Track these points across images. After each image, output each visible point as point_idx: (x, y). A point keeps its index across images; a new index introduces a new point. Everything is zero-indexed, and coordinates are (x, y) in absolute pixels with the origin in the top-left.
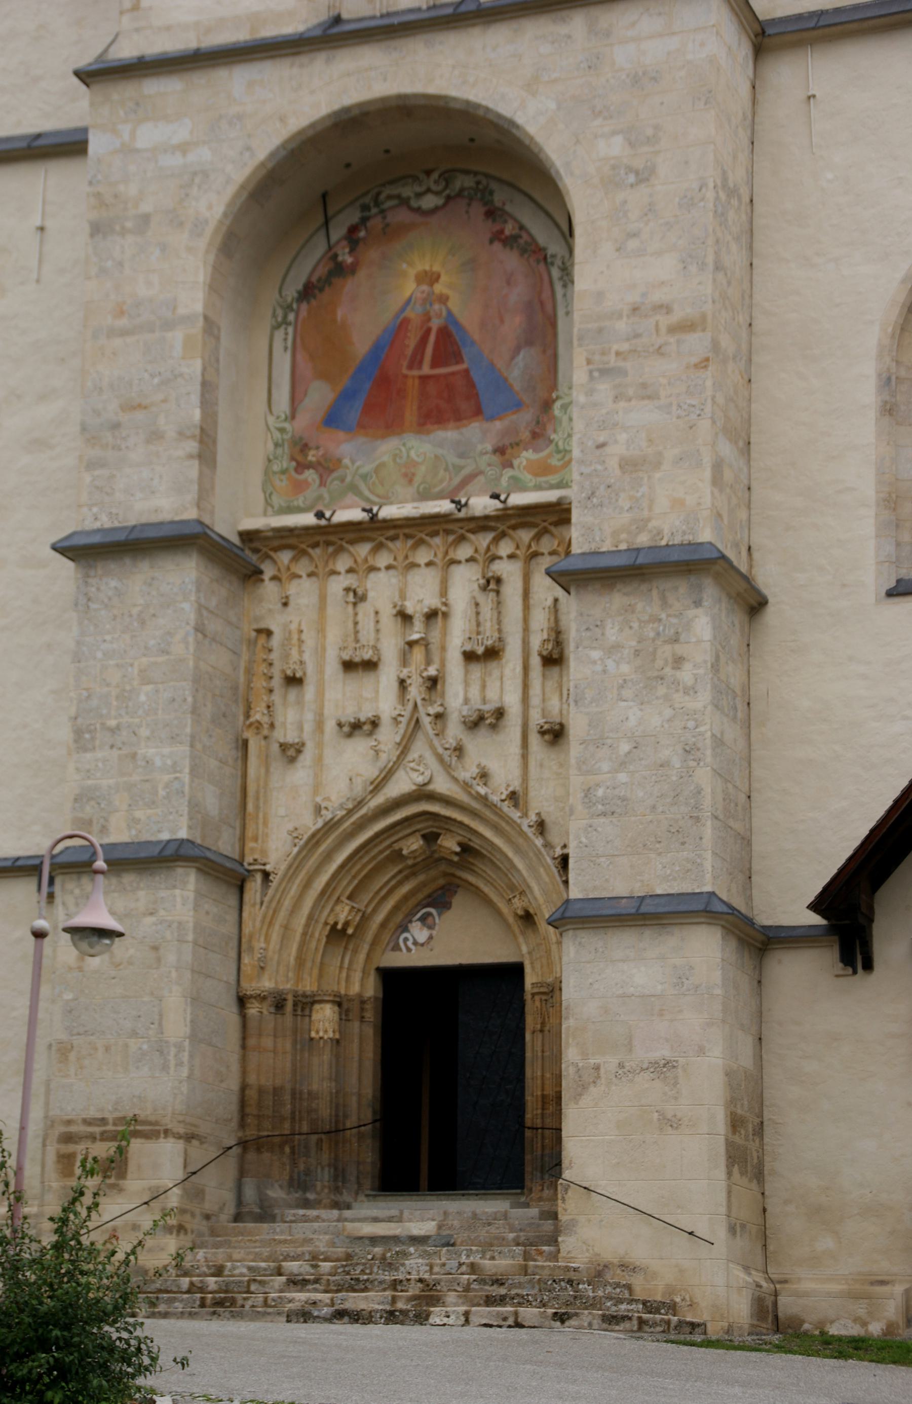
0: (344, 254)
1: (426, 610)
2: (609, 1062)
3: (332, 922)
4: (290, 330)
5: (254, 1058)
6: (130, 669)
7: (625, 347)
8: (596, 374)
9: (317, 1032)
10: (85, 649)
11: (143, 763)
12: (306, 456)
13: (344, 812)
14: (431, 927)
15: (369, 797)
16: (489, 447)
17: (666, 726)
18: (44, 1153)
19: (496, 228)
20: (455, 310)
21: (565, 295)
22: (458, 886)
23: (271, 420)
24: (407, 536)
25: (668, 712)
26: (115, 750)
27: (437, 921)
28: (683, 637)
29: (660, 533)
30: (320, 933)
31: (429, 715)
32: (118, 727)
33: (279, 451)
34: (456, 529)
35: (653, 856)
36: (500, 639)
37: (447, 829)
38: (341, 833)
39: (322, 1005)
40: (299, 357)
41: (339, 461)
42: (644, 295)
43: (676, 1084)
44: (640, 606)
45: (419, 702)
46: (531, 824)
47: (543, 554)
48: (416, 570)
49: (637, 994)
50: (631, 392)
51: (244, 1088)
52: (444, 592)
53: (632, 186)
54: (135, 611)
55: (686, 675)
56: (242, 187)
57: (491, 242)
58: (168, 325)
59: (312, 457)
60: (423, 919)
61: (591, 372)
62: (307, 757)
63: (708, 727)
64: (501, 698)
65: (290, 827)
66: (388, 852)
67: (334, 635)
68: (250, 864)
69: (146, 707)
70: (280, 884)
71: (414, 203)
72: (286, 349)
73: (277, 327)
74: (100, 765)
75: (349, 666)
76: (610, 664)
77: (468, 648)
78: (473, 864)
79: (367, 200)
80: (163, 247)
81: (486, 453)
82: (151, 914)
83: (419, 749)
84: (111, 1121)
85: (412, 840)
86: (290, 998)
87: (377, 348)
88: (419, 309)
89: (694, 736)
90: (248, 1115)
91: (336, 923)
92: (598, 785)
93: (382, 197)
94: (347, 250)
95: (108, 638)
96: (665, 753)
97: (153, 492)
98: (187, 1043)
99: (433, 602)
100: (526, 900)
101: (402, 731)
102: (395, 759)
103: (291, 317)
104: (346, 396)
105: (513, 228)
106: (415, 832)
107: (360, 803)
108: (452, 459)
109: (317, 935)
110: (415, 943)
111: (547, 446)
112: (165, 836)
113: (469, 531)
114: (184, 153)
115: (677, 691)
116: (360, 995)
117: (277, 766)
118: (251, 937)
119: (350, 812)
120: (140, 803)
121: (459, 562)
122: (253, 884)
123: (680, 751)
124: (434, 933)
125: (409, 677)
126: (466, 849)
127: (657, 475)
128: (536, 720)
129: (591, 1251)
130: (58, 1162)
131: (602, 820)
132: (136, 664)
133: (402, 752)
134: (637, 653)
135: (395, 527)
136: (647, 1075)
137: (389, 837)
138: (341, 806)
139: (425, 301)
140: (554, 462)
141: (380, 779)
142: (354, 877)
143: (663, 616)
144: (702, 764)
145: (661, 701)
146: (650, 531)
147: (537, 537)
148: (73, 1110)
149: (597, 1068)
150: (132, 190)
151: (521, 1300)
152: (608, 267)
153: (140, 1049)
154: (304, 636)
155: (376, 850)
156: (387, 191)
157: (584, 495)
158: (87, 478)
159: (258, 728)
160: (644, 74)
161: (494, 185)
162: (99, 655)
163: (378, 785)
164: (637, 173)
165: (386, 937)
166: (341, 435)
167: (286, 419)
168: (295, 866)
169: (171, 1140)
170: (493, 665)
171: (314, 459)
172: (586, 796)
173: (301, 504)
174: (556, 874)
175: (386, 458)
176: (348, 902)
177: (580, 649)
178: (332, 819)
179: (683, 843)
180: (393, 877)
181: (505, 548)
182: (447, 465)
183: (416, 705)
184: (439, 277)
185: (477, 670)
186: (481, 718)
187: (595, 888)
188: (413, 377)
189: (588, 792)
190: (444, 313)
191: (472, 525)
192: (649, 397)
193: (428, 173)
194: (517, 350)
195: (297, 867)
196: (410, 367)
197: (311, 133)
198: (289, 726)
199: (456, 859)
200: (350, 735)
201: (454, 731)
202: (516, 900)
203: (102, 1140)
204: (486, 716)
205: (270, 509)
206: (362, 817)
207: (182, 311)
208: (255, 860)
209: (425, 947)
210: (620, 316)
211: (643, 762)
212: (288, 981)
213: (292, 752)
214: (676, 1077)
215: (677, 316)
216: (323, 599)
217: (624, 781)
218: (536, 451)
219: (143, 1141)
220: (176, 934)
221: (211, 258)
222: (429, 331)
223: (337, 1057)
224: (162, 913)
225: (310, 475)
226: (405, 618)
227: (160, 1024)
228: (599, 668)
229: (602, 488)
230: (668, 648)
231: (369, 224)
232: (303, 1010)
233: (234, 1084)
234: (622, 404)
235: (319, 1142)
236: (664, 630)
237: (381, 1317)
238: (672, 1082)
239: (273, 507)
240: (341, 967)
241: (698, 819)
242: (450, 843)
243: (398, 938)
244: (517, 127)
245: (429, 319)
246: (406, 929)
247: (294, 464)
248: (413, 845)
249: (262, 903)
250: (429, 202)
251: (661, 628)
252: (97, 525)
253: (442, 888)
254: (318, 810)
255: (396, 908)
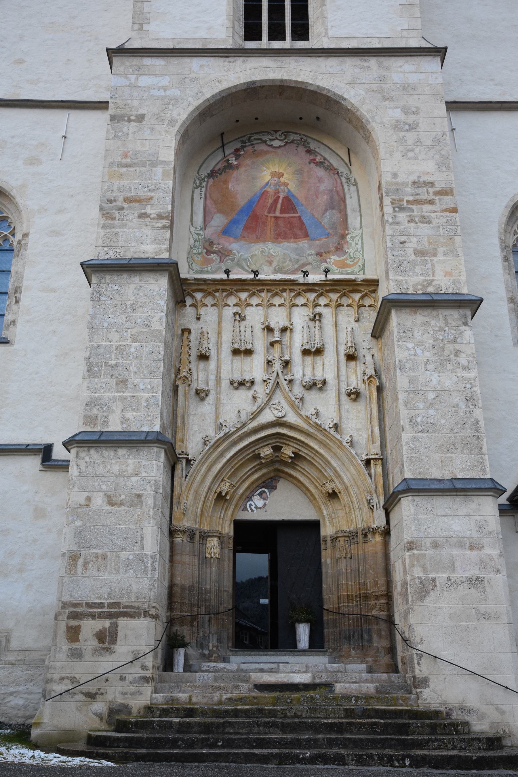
0: (232, 160)
1: (281, 327)
2: (441, 577)
3: (218, 492)
4: (203, 190)
5: (179, 568)
6: (125, 334)
7: (411, 198)
8: (397, 209)
9: (210, 554)
10: (96, 321)
11: (132, 386)
12: (213, 247)
13: (235, 429)
14: (264, 499)
15: (249, 422)
16: (313, 252)
17: (454, 386)
18: (56, 625)
19: (312, 157)
20: (292, 190)
21: (349, 190)
22: (280, 478)
23: (192, 229)
24: (269, 291)
25: (455, 379)
26: (113, 377)
27: (268, 496)
28: (459, 340)
29: (440, 287)
30: (212, 497)
31: (286, 380)
32: (116, 365)
33: (197, 244)
34: (297, 289)
35: (454, 456)
36: (323, 345)
37: (286, 444)
38: (231, 441)
39: (213, 538)
40: (208, 202)
41: (231, 251)
42: (419, 177)
43: (484, 591)
44: (433, 322)
45: (280, 373)
46: (348, 441)
47: (343, 306)
48: (273, 308)
49: (455, 536)
50: (417, 219)
51: (171, 587)
52: (290, 317)
53: (407, 130)
54: (129, 303)
55: (463, 360)
56: (197, 108)
57: (310, 163)
58: (153, 164)
59: (215, 248)
60: (260, 494)
61: (394, 208)
62: (211, 399)
63: (478, 388)
64: (323, 375)
65: (201, 435)
66: (252, 455)
67: (227, 337)
68: (179, 454)
69: (135, 355)
70: (197, 467)
71: (269, 143)
72: (201, 198)
73: (194, 188)
74: (104, 385)
75: (236, 352)
76: (419, 351)
77: (306, 347)
78: (297, 465)
79: (244, 139)
80: (152, 130)
81: (312, 255)
82: (137, 474)
83: (278, 397)
84: (106, 605)
85: (266, 449)
86: (197, 533)
87: (250, 202)
88: (273, 188)
89: (471, 392)
90: (175, 602)
91: (221, 493)
92: (417, 415)
93: (252, 138)
94: (234, 159)
95: (111, 316)
96: (455, 401)
97: (142, 243)
98: (158, 556)
99: (283, 322)
100: (333, 484)
101: (270, 388)
102: (265, 402)
103: (204, 184)
104: (234, 222)
105: (320, 159)
106: (268, 444)
107: (244, 424)
108: (294, 256)
109: (211, 498)
110: (256, 507)
111: (345, 255)
112: (146, 429)
113: (303, 291)
114: (165, 90)
115: (459, 368)
116: (227, 534)
117: (193, 402)
118: (179, 496)
119: (238, 429)
120: (130, 409)
121: (298, 306)
122: (180, 466)
123: (464, 400)
124: (267, 502)
125: (274, 359)
126: (297, 456)
127: (435, 259)
128: (344, 387)
129: (440, 699)
130: (67, 631)
131: (422, 435)
132: (129, 331)
133: (269, 400)
134: (434, 347)
135: (263, 285)
136: (466, 586)
137: (254, 446)
138: (234, 426)
139: (275, 185)
140: (349, 262)
141: (257, 412)
142: (232, 467)
143: (447, 328)
144: (477, 407)
145: (450, 372)
146: (434, 286)
147: (341, 297)
148: (80, 596)
149: (434, 580)
150: (136, 103)
151: (440, 743)
152: (398, 163)
153: (128, 558)
154: (209, 335)
155: (246, 453)
156: (255, 136)
157: (395, 265)
158: (102, 233)
159: (184, 380)
160: (409, 86)
161: (309, 140)
162: (106, 324)
163: (255, 416)
164: (409, 125)
165: (241, 503)
166: (232, 239)
167: (201, 230)
168: (206, 457)
169: (148, 619)
170: (318, 358)
171: (216, 249)
172: (411, 421)
173: (209, 270)
174: (364, 469)
175: (256, 252)
176: (228, 480)
177: (400, 342)
178: (229, 432)
179: (471, 450)
180: (251, 469)
181: (323, 301)
182: (291, 258)
183: (278, 374)
184: (283, 175)
185: (309, 360)
186: (315, 384)
187: (420, 473)
188: (271, 217)
189: (411, 419)
190: (286, 191)
191: (306, 288)
192: (427, 223)
193: (276, 132)
194: (326, 210)
195: (206, 458)
196: (269, 212)
197: (234, 90)
198: (200, 382)
199: (290, 461)
200: (237, 388)
201: (298, 390)
202: (327, 485)
203: (99, 617)
204: (318, 383)
205: (191, 271)
206: (244, 433)
207: (161, 159)
208: (183, 452)
209: (262, 509)
210: (408, 185)
211: (443, 404)
212: (196, 524)
213: (203, 395)
214: (484, 587)
215: (437, 188)
216: (220, 317)
217: (433, 414)
218: (338, 256)
219: (129, 619)
220: (153, 488)
221: (178, 137)
222: (279, 197)
223: (218, 569)
224: (144, 474)
225: (214, 256)
226: (269, 329)
227: (142, 544)
228: (412, 353)
229: (405, 263)
230: (451, 345)
231: (245, 149)
232: (203, 540)
233: (166, 583)
234: (412, 224)
235: (210, 620)
236: (448, 336)
237: (352, 760)
238: (482, 590)
239: (193, 270)
240: (220, 518)
241: (478, 437)
242: (288, 451)
243: (246, 504)
244: (345, 99)
245: (279, 192)
246: (251, 499)
247: (205, 250)
248: (267, 452)
249: (186, 476)
250: (277, 143)
251: (446, 335)
252: (108, 257)
253: (271, 478)
254: (220, 427)
255: (248, 487)
